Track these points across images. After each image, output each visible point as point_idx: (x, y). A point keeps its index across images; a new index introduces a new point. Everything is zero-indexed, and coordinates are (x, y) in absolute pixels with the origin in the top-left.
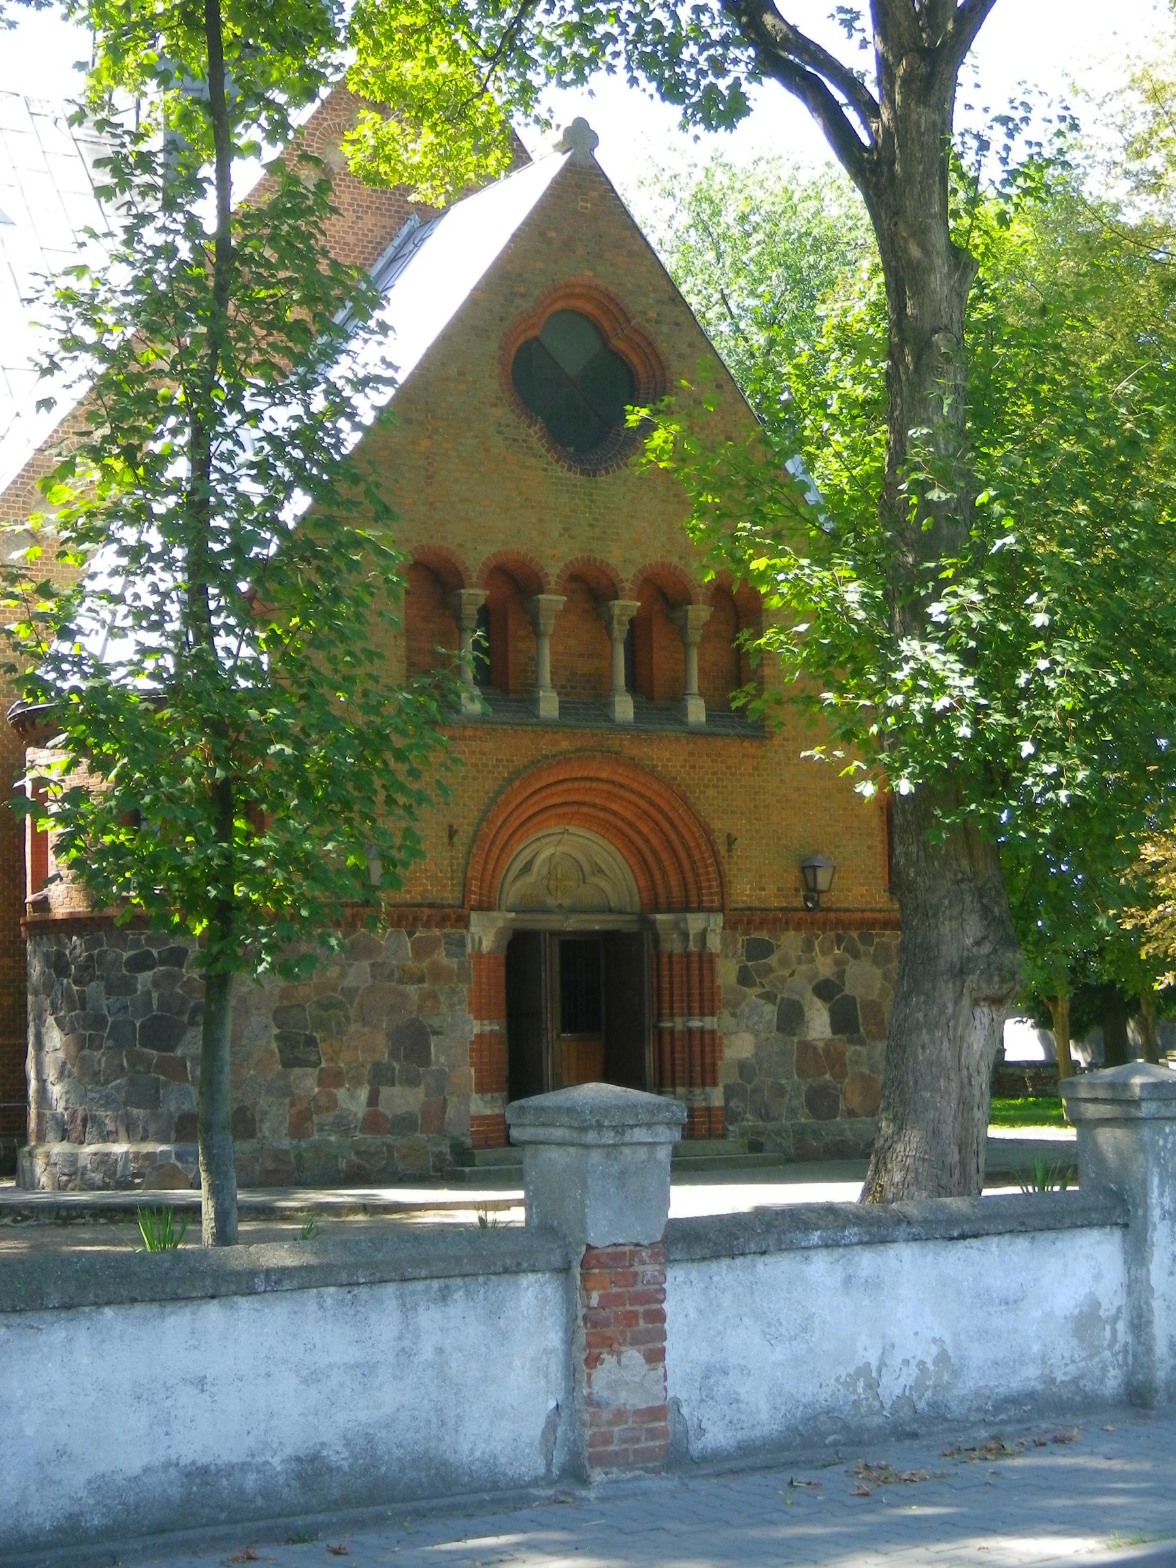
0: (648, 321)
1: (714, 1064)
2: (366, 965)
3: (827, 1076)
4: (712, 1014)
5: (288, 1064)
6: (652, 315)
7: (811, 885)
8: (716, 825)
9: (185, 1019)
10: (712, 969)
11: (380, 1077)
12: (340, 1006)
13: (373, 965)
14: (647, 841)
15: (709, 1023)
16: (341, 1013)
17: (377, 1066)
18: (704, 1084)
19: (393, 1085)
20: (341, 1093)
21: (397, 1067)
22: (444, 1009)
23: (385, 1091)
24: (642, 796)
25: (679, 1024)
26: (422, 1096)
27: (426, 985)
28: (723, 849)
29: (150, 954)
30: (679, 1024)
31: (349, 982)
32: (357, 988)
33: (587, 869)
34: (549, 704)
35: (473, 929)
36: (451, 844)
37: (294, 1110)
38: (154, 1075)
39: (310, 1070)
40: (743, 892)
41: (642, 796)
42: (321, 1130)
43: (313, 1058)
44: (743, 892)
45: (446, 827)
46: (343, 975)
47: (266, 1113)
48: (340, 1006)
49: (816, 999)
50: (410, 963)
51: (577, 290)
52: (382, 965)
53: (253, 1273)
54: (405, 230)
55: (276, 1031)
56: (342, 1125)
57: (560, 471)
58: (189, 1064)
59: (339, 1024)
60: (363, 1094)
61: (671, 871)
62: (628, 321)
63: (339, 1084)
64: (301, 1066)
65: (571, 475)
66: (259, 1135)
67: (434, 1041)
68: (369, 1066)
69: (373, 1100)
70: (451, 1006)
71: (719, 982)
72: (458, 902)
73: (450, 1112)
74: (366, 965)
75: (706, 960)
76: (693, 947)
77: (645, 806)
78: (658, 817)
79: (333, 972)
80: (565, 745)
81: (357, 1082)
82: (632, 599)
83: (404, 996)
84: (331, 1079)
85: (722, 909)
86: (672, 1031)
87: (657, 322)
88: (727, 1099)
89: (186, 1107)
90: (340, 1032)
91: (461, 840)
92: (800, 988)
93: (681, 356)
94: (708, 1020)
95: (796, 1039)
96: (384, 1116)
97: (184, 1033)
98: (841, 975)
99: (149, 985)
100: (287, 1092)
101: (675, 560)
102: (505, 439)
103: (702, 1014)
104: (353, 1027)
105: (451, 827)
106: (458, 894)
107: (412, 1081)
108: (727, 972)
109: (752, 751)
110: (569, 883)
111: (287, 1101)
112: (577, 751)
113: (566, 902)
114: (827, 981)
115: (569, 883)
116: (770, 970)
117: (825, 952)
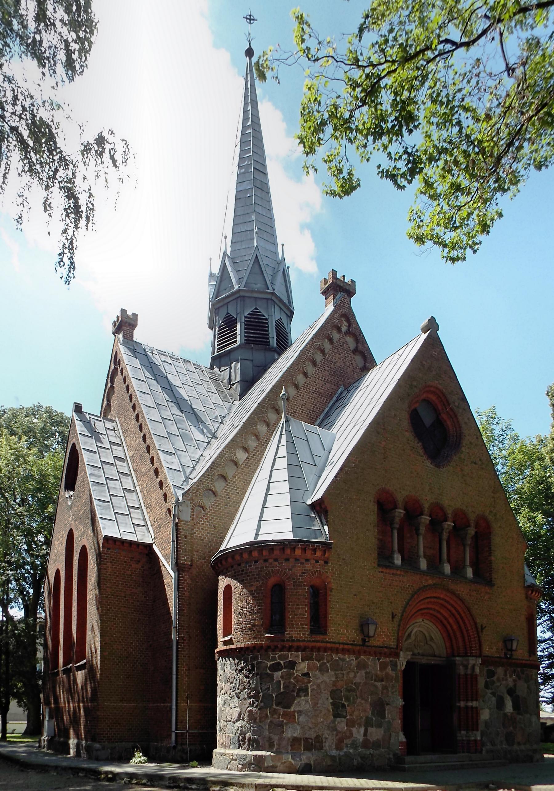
0: (455, 406)
1: (477, 721)
2: (363, 672)
3: (511, 728)
4: (476, 700)
5: (336, 716)
6: (457, 404)
7: (509, 647)
8: (478, 621)
9: (295, 694)
10: (476, 681)
11: (368, 724)
12: (354, 690)
13: (366, 673)
14: (451, 627)
15: (474, 704)
16: (355, 694)
17: (367, 718)
18: (473, 730)
19: (373, 727)
20: (354, 730)
21: (374, 719)
22: (390, 694)
23: (370, 730)
24: (453, 606)
25: (462, 704)
26: (382, 732)
27: (384, 683)
28: (480, 630)
29: (279, 663)
30: (462, 704)
31: (357, 680)
32: (360, 683)
33: (428, 638)
34: (423, 564)
35: (401, 659)
36: (393, 621)
37: (337, 737)
38: (281, 719)
39: (343, 719)
40: (487, 650)
41: (453, 606)
42: (347, 747)
43: (345, 714)
44: (487, 650)
45: (391, 613)
46: (355, 677)
47: (326, 738)
48: (354, 690)
49: (508, 696)
50: (378, 672)
51: (432, 389)
52: (369, 673)
53: (244, 784)
54: (339, 391)
55: (331, 701)
56: (354, 745)
57: (428, 463)
58: (296, 715)
59: (353, 698)
60: (362, 730)
61: (460, 640)
62: (449, 405)
63: (354, 726)
64: (339, 717)
65: (431, 466)
66: (324, 748)
67: (387, 707)
68: (364, 718)
69: (365, 734)
70: (393, 693)
71: (479, 686)
72: (395, 647)
73: (392, 741)
74: (363, 672)
75: (474, 677)
76: (469, 672)
77: (454, 611)
78: (458, 616)
79: (352, 675)
80: (430, 582)
81: (360, 726)
82: (451, 522)
83: (376, 687)
84: (351, 724)
85: (480, 656)
86: (459, 707)
87: (458, 407)
88: (482, 737)
89: (295, 735)
90: (354, 703)
91: (397, 619)
92: (503, 691)
93: (466, 423)
94: (474, 703)
95: (502, 712)
96: (369, 740)
97: (294, 700)
98: (515, 686)
99: (279, 677)
100: (334, 729)
101: (464, 508)
102: (410, 446)
103: (472, 700)
104: (359, 700)
105: (393, 613)
106: (395, 643)
107: (379, 726)
108: (481, 682)
109: (488, 591)
110: (421, 644)
111: (335, 733)
112: (434, 585)
113: (421, 652)
114: (511, 688)
115: (421, 644)
116: (494, 682)
117: (511, 676)
